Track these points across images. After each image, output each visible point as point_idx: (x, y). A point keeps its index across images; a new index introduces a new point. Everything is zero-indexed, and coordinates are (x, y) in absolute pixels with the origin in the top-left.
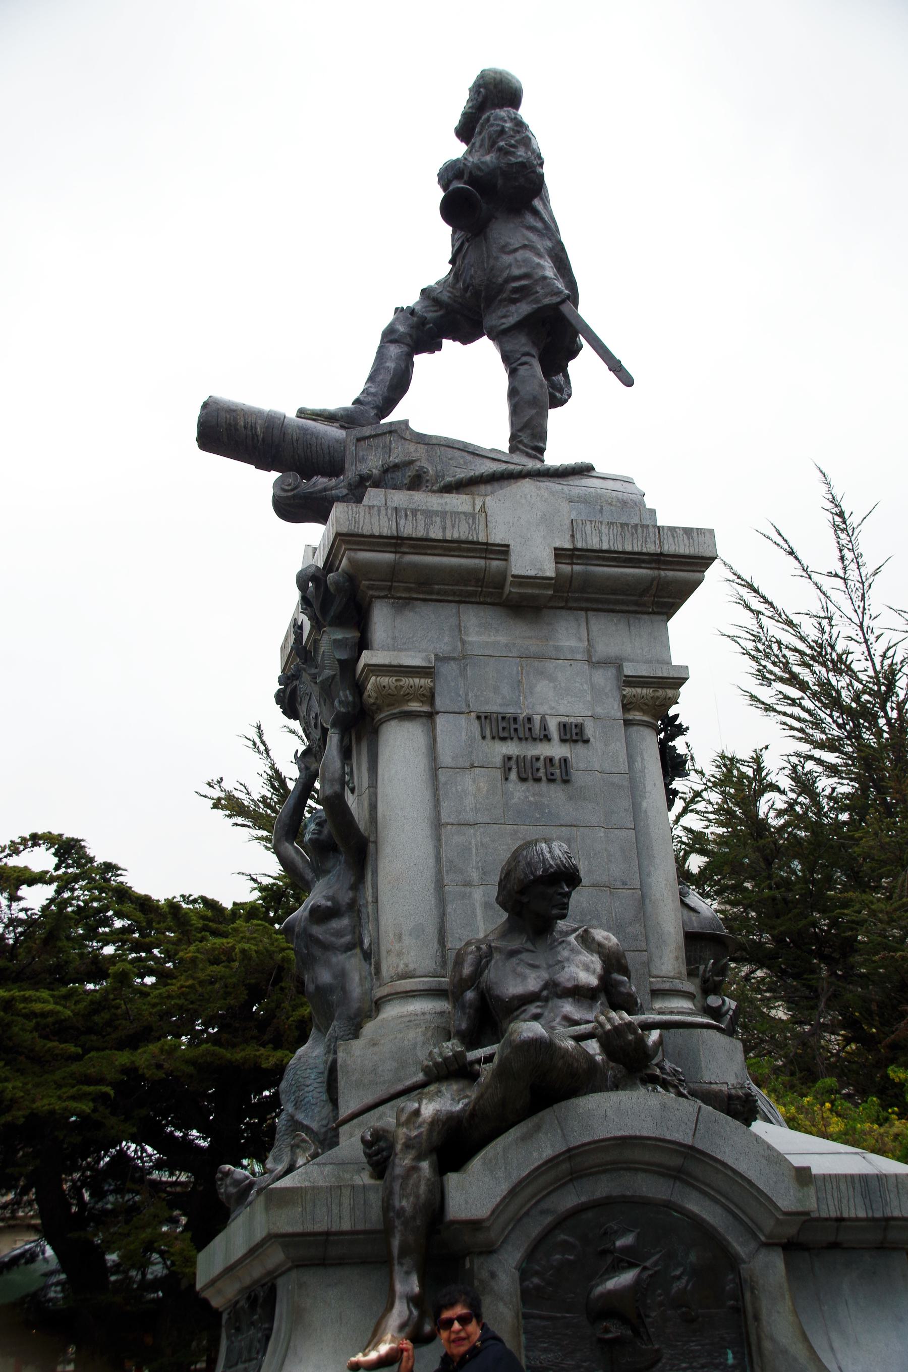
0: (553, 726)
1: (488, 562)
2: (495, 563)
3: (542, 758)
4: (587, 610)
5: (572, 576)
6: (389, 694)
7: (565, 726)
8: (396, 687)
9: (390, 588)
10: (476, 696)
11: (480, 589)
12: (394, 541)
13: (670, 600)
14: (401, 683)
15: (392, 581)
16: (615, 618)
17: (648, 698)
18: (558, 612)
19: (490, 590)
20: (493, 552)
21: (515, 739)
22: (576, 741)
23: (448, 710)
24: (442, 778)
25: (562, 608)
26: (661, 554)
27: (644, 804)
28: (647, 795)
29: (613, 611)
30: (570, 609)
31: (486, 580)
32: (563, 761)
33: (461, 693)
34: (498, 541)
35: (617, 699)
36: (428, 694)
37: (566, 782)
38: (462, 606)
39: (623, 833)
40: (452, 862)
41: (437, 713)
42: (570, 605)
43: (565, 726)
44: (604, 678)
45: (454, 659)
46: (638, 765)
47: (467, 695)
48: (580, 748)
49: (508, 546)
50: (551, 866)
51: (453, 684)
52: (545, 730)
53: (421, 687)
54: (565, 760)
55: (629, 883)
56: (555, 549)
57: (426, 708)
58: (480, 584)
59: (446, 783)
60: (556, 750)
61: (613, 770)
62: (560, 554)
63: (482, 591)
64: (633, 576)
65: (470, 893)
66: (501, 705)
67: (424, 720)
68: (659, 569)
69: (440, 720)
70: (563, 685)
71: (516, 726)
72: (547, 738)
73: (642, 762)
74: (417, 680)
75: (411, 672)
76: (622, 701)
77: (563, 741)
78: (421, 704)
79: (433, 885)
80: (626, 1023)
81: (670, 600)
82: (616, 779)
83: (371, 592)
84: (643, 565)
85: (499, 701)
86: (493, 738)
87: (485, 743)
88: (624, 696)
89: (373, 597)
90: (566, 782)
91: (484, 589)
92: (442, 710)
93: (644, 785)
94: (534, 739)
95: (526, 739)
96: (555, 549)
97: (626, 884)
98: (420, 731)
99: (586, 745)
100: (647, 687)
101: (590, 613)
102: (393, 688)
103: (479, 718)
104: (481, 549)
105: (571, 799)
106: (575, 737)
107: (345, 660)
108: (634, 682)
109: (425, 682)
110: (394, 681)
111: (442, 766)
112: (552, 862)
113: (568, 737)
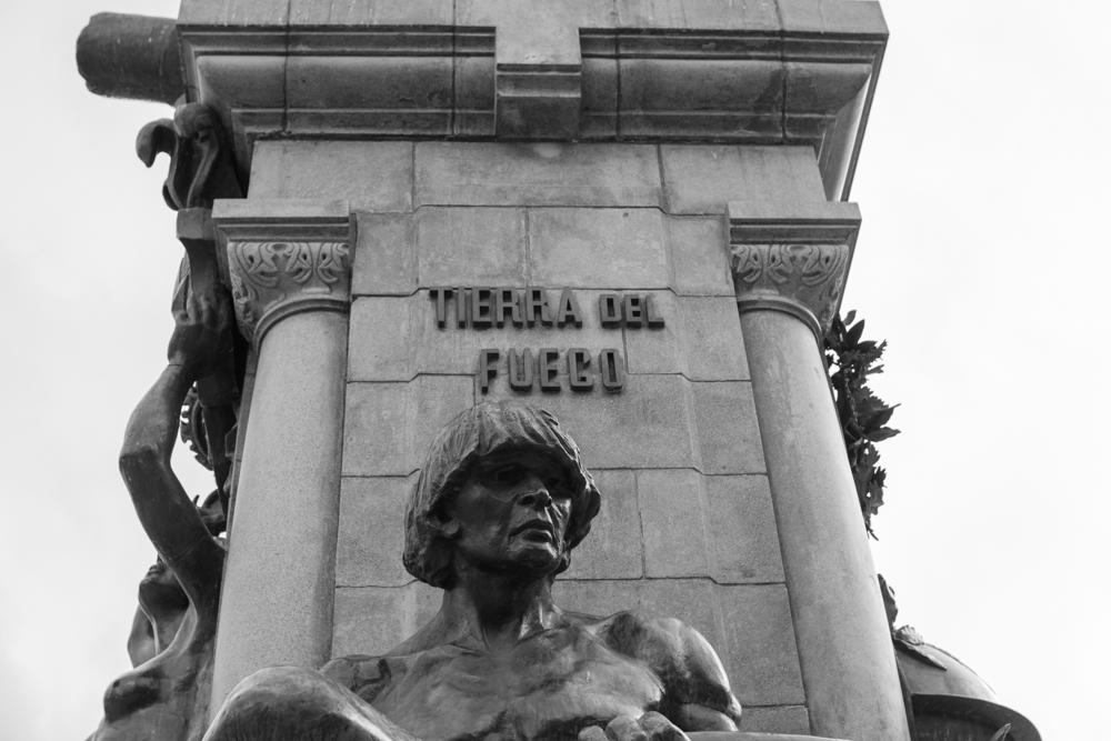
0: (587, 306)
1: (458, 59)
2: (470, 64)
3: (562, 355)
4: (657, 141)
5: (619, 76)
6: (263, 273)
7: (610, 302)
8: (275, 258)
9: (284, 119)
10: (432, 265)
11: (450, 111)
12: (283, 34)
13: (815, 116)
14: (286, 251)
15: (284, 104)
16: (715, 152)
17: (784, 259)
18: (604, 147)
19: (470, 111)
20: (466, 42)
21: (509, 324)
22: (635, 326)
23: (375, 292)
24: (351, 400)
25: (611, 140)
26: (782, 33)
27: (789, 436)
28: (795, 421)
29: (708, 141)
30: (628, 140)
31: (457, 91)
32: (605, 358)
33: (405, 265)
34: (475, 22)
35: (723, 265)
36: (338, 268)
37: (614, 391)
38: (420, 147)
39: (742, 483)
40: (355, 542)
41: (355, 297)
42: (626, 132)
43: (610, 302)
44: (699, 238)
45: (395, 215)
46: (773, 371)
47: (416, 264)
48: (644, 337)
49: (492, 30)
50: (496, 436)
51: (389, 253)
52: (569, 308)
53: (324, 257)
54: (611, 356)
55: (758, 572)
56: (582, 31)
57: (338, 296)
58: (449, 100)
59: (358, 407)
60: (595, 341)
61: (718, 376)
62: (588, 39)
63: (453, 114)
64: (735, 70)
65: (391, 600)
66: (481, 277)
67: (336, 317)
68: (783, 59)
69: (357, 309)
70: (609, 243)
71: (508, 305)
72: (572, 322)
73: (781, 368)
74: (315, 246)
75: (306, 231)
76: (734, 270)
77: (608, 326)
78: (327, 289)
79: (311, 591)
80: (657, 736)
81: (815, 116)
82: (724, 390)
83: (248, 129)
84: (752, 54)
85: (479, 270)
86: (462, 325)
87: (443, 335)
88: (736, 259)
89: (253, 137)
90: (614, 391)
91: (457, 111)
92: (363, 292)
93: (788, 404)
94: (548, 325)
95: (531, 325)
96: (582, 31)
97: (751, 576)
98: (321, 332)
99: (657, 333)
100: (781, 243)
101: (664, 148)
102: (268, 259)
103: (434, 294)
104: (444, 38)
105: (623, 422)
106: (630, 318)
107: (199, 241)
108: (755, 233)
109: (335, 248)
110: (269, 248)
111: (354, 378)
112: (499, 426)
113: (618, 317)
